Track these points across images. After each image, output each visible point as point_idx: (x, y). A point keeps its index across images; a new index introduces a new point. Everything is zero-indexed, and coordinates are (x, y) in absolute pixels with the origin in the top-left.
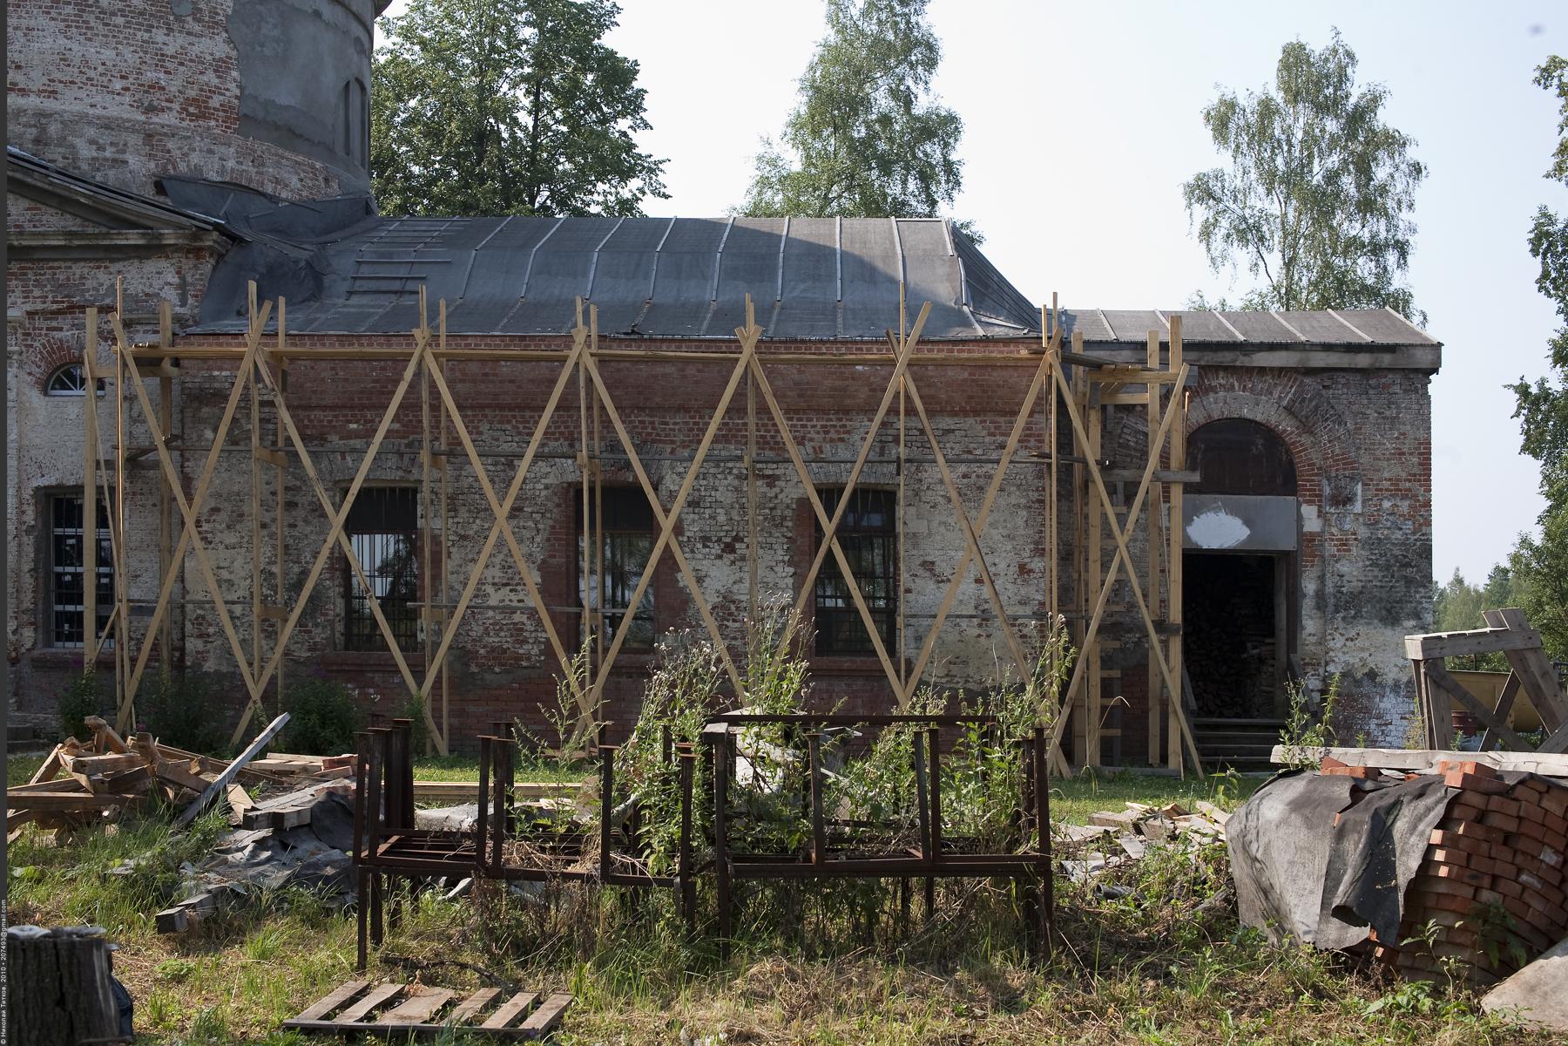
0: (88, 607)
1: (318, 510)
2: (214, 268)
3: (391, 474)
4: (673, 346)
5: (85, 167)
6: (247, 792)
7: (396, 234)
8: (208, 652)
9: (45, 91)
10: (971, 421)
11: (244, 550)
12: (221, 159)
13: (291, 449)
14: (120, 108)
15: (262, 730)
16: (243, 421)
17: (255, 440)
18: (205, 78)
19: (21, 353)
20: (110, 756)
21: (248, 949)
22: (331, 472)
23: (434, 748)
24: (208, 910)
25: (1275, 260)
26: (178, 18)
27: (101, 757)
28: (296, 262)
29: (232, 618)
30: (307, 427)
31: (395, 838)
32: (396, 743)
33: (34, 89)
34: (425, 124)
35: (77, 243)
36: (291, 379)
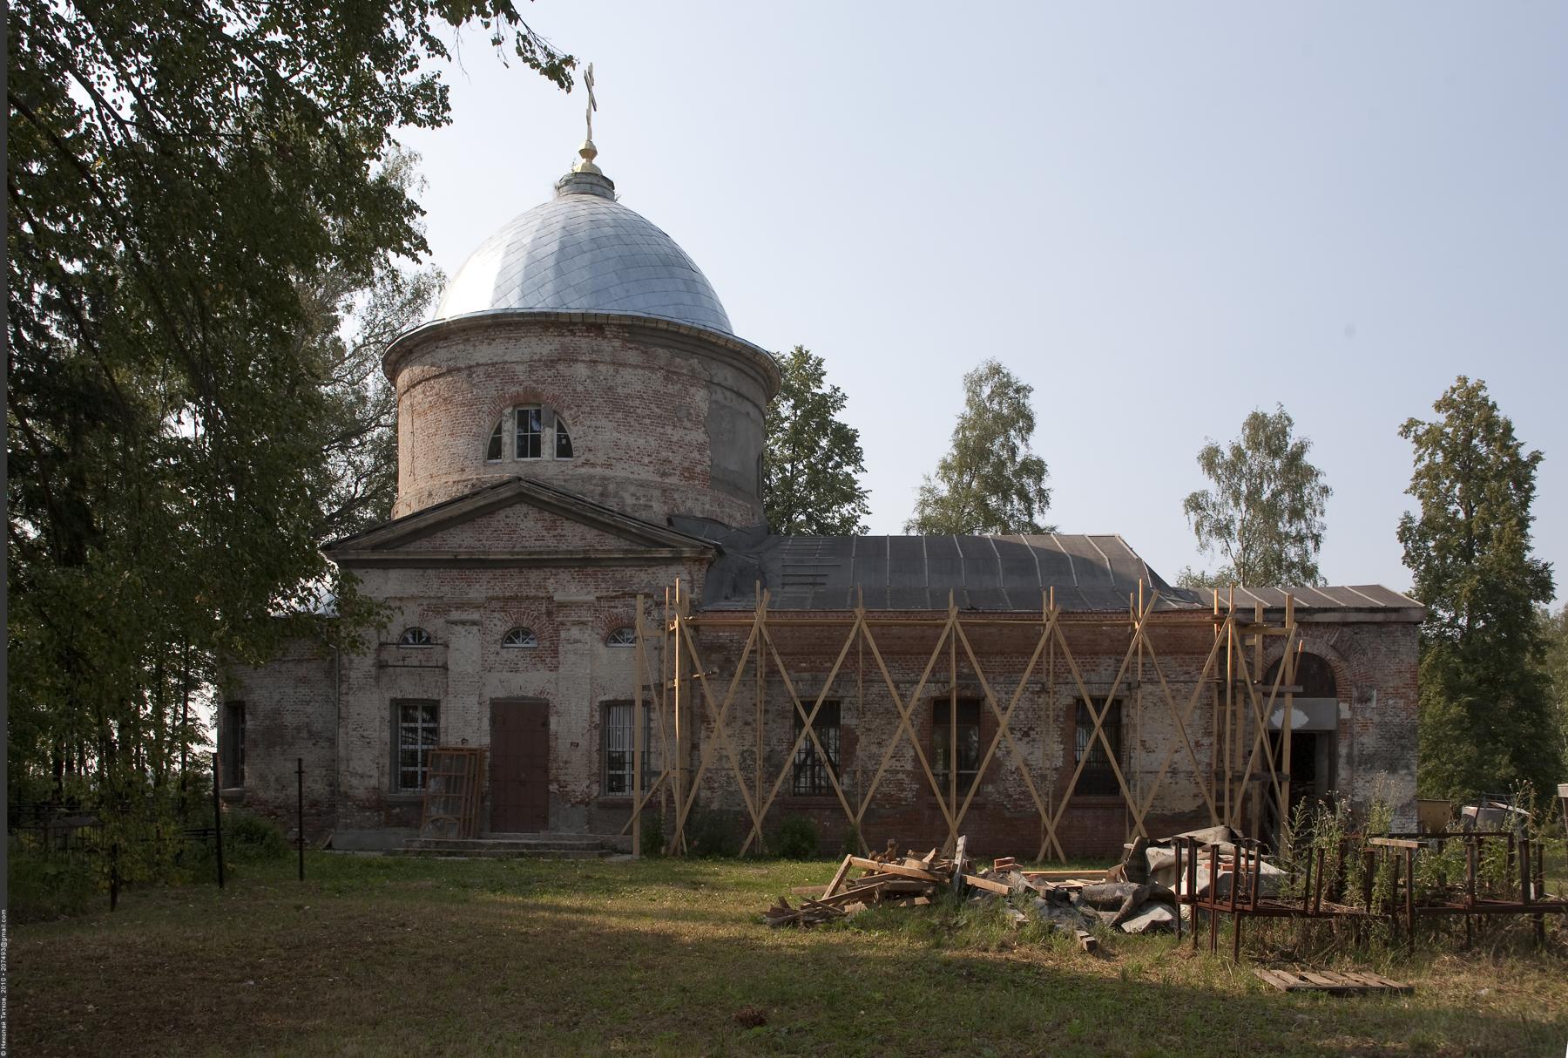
4: (996, 616)
5: (629, 510)
10: (1169, 658)
14: (646, 474)
25: (1236, 546)
26: (680, 419)
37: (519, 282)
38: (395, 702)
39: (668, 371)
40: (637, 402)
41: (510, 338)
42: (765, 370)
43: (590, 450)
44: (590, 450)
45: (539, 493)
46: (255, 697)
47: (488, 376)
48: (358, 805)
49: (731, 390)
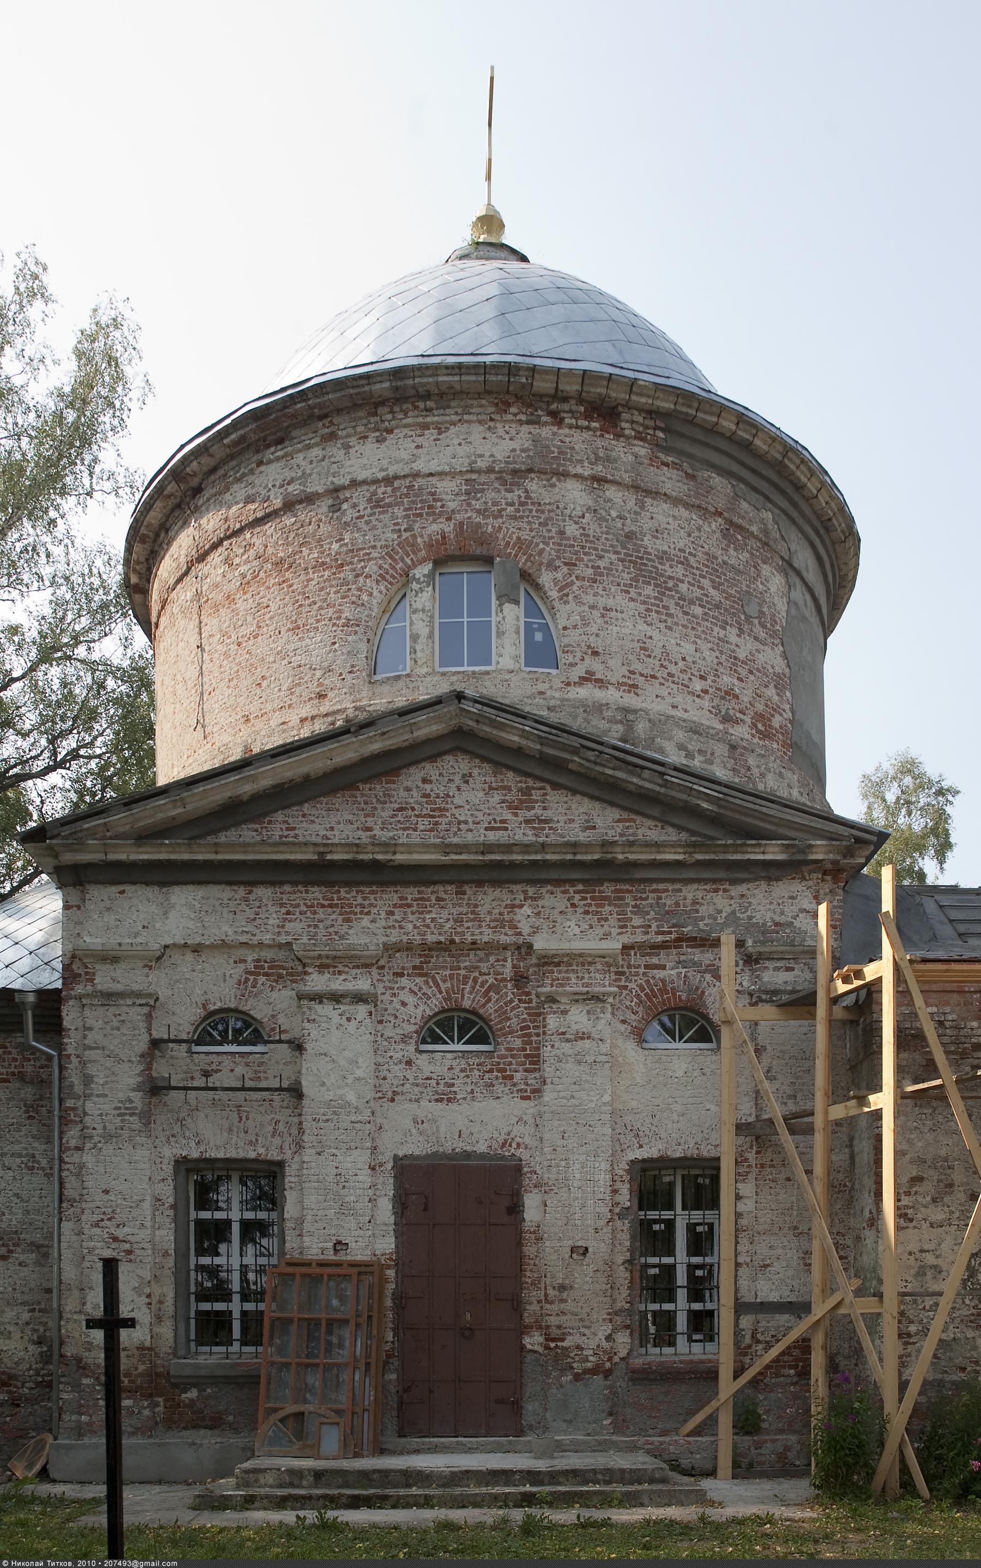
9: (624, 684)
11: (954, 1228)
33: (613, 680)
38: (184, 1166)
39: (730, 523)
40: (680, 571)
41: (425, 426)
43: (595, 653)
44: (595, 653)
45: (502, 726)
47: (377, 504)
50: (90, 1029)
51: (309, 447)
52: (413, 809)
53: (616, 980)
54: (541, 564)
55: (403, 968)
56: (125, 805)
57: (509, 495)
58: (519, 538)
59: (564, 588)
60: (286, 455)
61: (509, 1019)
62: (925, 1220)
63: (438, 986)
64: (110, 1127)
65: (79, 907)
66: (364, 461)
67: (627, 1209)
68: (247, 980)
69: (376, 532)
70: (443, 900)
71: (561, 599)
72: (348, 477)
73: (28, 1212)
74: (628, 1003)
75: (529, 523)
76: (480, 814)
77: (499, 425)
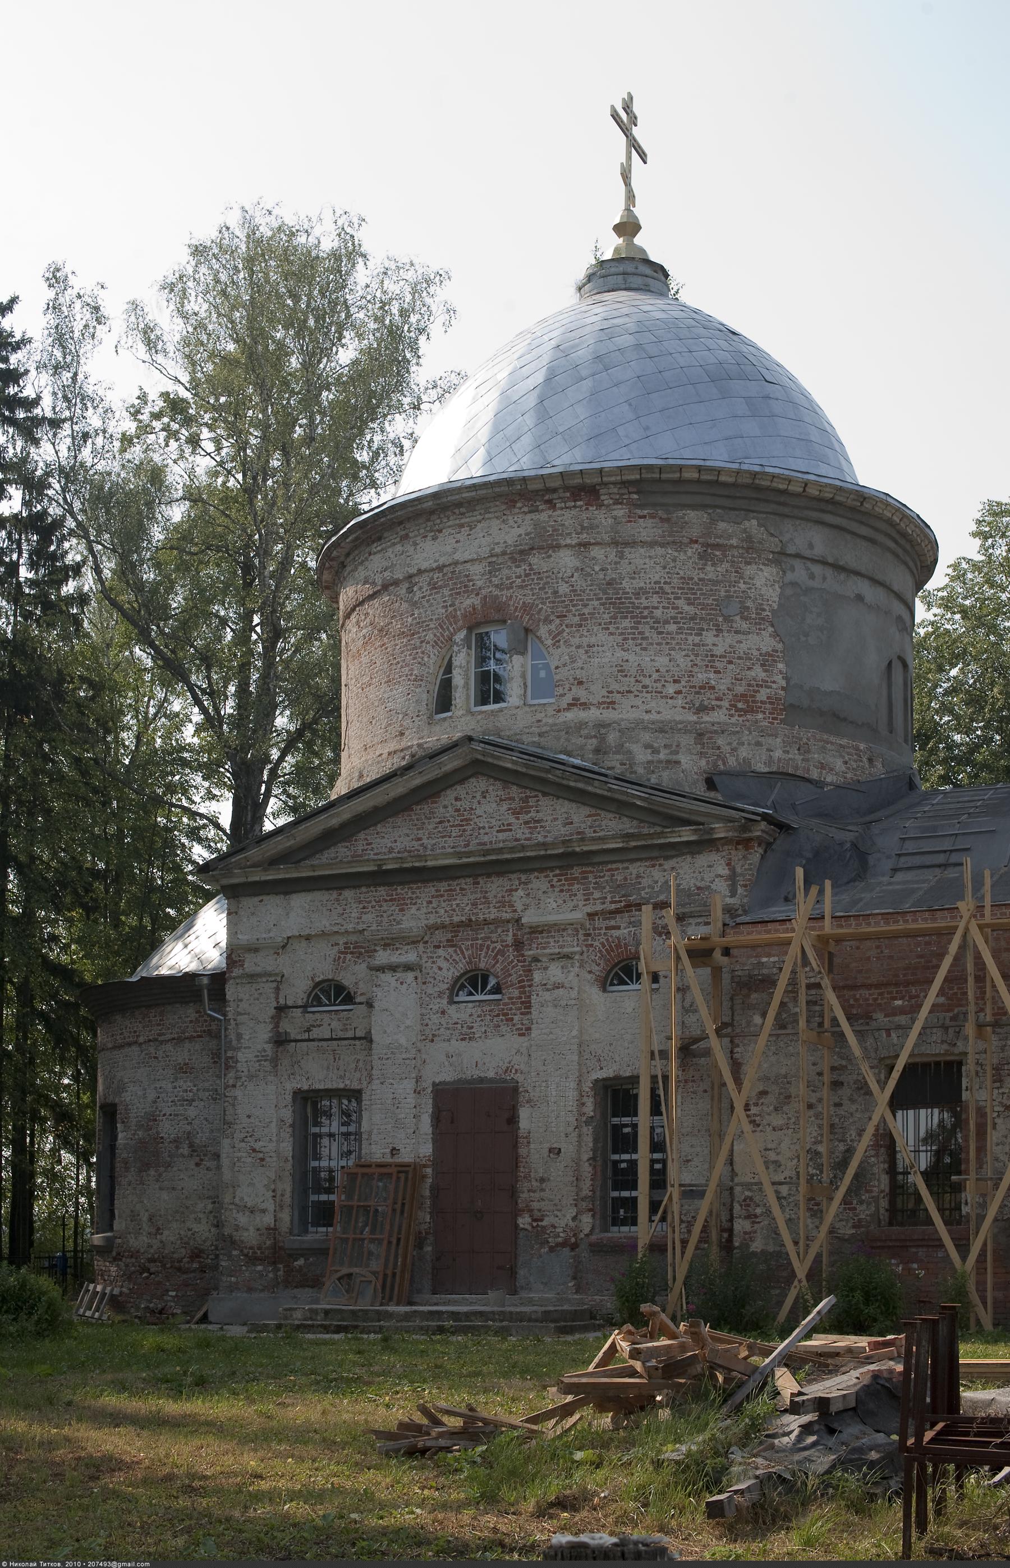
0: (642, 1193)
1: (863, 1088)
2: (763, 857)
3: (936, 1049)
5: (641, 770)
6: (794, 1375)
7: (939, 807)
8: (755, 1232)
9: (604, 703)
12: (769, 750)
13: (837, 1029)
14: (674, 711)
15: (809, 1313)
16: (791, 1005)
17: (802, 1023)
18: (753, 673)
19: (582, 954)
20: (664, 1342)
21: (794, 1535)
22: (876, 1050)
23: (978, 1322)
24: (755, 1496)
26: (727, 619)
27: (655, 1344)
28: (841, 844)
29: (779, 1198)
30: (852, 1006)
31: (940, 1426)
32: (943, 1329)
33: (595, 702)
34: (967, 692)
35: (633, 844)
36: (837, 960)
37: (484, 441)
41: (462, 526)
42: (890, 522)
43: (580, 683)
44: (580, 683)
45: (499, 758)
46: (127, 1097)
47: (434, 587)
48: (246, 1255)
49: (824, 563)
50: (241, 1000)
51: (394, 544)
52: (449, 821)
53: (584, 941)
54: (540, 620)
55: (440, 942)
56: (257, 842)
57: (518, 570)
58: (524, 603)
59: (556, 637)
60: (382, 550)
61: (510, 975)
62: (769, 1125)
63: (463, 953)
64: (252, 1070)
65: (236, 913)
66: (425, 555)
67: (592, 1117)
68: (339, 957)
69: (433, 608)
70: (464, 889)
71: (554, 645)
72: (416, 568)
73: (213, 1131)
74: (593, 957)
75: (532, 589)
76: (493, 821)
77: (510, 518)
